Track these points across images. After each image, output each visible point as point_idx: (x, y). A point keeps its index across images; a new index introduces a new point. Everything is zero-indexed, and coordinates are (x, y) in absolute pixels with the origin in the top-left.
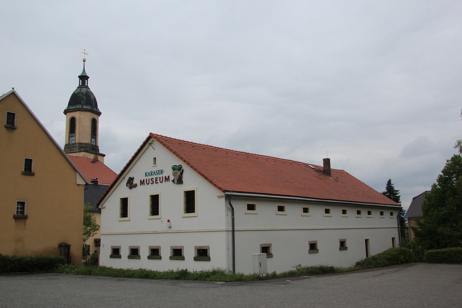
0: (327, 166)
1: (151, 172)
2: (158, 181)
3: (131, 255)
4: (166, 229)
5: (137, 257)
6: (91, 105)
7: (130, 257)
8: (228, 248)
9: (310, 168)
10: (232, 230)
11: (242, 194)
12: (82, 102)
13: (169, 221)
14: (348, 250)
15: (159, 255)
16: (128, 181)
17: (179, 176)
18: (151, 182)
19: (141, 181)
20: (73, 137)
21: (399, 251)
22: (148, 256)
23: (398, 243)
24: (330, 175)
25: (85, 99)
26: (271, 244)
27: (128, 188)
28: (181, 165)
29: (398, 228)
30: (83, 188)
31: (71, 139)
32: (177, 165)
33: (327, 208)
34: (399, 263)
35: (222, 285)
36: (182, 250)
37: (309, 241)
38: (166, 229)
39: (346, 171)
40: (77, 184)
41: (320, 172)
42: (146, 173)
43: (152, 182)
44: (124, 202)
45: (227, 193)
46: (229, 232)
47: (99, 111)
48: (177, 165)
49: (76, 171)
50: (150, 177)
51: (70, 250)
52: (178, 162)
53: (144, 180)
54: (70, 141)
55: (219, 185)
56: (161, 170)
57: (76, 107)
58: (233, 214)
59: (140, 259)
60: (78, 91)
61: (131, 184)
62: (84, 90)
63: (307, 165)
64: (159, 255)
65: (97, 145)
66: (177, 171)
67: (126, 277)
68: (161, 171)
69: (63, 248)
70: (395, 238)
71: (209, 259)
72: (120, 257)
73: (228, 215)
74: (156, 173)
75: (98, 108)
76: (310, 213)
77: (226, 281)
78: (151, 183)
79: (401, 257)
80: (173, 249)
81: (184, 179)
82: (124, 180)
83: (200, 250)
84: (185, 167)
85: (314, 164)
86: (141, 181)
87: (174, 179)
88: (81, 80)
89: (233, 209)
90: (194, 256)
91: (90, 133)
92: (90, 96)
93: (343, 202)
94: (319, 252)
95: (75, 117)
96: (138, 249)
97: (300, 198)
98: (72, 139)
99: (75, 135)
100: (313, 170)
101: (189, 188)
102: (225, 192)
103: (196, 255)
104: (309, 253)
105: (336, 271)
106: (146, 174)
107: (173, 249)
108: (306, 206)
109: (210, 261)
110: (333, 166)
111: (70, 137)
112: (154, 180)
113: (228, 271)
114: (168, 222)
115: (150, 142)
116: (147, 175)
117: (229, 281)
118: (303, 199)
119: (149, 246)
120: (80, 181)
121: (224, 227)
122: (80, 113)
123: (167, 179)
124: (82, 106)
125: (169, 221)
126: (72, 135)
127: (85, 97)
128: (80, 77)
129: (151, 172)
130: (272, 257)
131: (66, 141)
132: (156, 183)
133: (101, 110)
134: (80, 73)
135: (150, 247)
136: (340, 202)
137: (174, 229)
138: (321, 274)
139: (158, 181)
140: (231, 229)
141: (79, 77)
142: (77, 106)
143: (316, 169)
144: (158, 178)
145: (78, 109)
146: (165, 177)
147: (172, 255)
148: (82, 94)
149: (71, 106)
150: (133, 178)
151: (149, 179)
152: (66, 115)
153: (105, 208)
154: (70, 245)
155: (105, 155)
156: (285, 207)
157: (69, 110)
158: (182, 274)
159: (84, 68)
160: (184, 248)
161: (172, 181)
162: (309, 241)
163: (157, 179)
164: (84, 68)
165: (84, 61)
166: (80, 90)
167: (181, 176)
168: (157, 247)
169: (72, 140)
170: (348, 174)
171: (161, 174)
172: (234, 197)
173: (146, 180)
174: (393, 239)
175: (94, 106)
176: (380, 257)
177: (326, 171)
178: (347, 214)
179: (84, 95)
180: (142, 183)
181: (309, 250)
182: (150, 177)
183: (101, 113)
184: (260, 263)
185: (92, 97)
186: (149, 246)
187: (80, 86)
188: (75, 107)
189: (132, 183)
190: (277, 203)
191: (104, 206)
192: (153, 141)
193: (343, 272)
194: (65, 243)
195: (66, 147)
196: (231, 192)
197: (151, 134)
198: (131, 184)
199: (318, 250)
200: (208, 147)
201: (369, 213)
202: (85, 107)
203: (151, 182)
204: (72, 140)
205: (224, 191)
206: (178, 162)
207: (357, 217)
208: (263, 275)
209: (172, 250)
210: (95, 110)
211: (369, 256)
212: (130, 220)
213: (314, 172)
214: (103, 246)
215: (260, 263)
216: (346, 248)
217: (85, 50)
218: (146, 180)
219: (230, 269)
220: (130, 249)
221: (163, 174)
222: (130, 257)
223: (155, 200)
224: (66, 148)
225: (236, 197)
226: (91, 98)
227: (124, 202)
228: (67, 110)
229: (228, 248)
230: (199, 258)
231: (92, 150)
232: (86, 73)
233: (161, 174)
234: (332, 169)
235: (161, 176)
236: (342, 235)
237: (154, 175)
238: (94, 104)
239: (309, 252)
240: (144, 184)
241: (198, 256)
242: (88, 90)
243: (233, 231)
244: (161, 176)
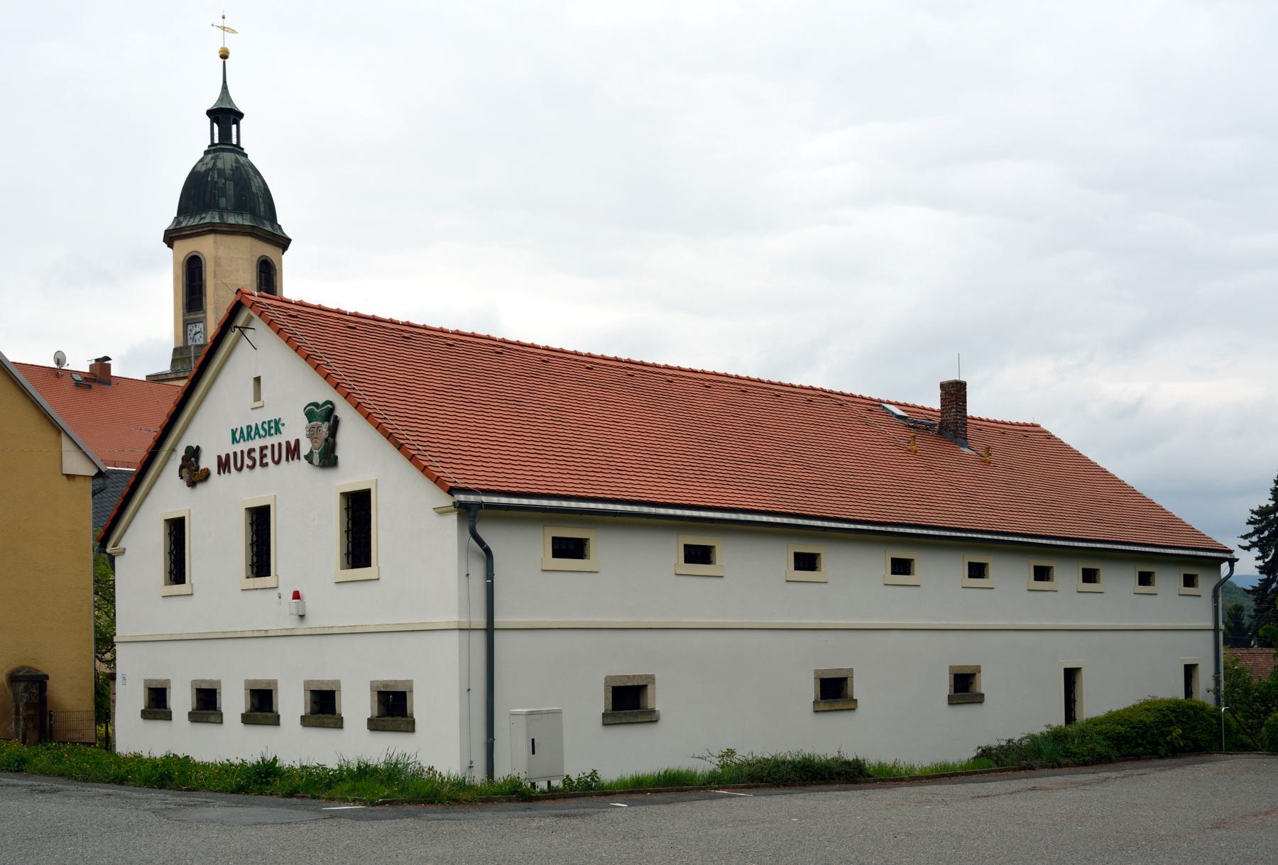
0: (952, 408)
1: (248, 427)
2: (268, 460)
3: (197, 709)
4: (290, 623)
5: (212, 718)
6: (253, 213)
7: (247, 719)
8: (469, 690)
9: (890, 414)
10: (485, 627)
11: (534, 502)
12: (223, 201)
13: (296, 595)
14: (985, 702)
15: (271, 711)
16: (183, 459)
17: (326, 440)
18: (248, 462)
19: (219, 457)
20: (198, 324)
21: (1168, 712)
22: (244, 712)
23: (1212, 685)
24: (964, 441)
25: (232, 192)
26: (651, 678)
27: (182, 484)
28: (331, 403)
29: (1216, 630)
30: (88, 487)
31: (191, 331)
32: (321, 403)
33: (1146, 568)
34: (1162, 753)
35: (355, 817)
36: (336, 692)
37: (816, 671)
38: (290, 623)
39: (1044, 426)
40: (64, 472)
41: (927, 429)
42: (232, 430)
43: (250, 463)
44: (176, 529)
45: (462, 498)
46: (472, 632)
47: (283, 233)
48: (321, 403)
49: (59, 430)
50: (244, 446)
51: (48, 693)
52: (322, 393)
53: (228, 456)
54: (189, 336)
55: (438, 470)
56: (275, 420)
57: (201, 219)
58: (490, 573)
59: (221, 722)
60: (207, 164)
61: (193, 473)
62: (227, 159)
63: (880, 406)
64: (274, 709)
66: (320, 423)
67: (109, 783)
68: (277, 422)
69: (21, 686)
70: (1200, 667)
71: (409, 727)
72: (338, 724)
73: (468, 575)
74: (262, 433)
75: (279, 223)
76: (1055, 581)
77: (373, 804)
78: (248, 466)
79: (1170, 733)
80: (313, 692)
81: (340, 452)
82: (173, 457)
83: (388, 693)
84: (344, 411)
85: (910, 402)
86: (219, 457)
87: (311, 452)
88: (216, 126)
89: (488, 552)
90: (369, 716)
92: (249, 179)
93: (970, 535)
94: (857, 710)
95: (202, 255)
96: (216, 690)
97: (778, 520)
98: (194, 332)
99: (205, 318)
100: (901, 421)
101: (354, 483)
102: (455, 496)
103: (376, 713)
104: (816, 711)
105: (869, 776)
106: (234, 433)
107: (312, 692)
108: (978, 558)
109: (413, 731)
110: (975, 407)
111: (186, 324)
112: (257, 455)
113: (356, 765)
114: (294, 598)
115: (240, 321)
116: (238, 439)
117: (383, 804)
118: (793, 521)
119: (246, 681)
120: (75, 463)
121: (452, 617)
122: (215, 242)
123: (293, 451)
124: (221, 217)
125: (296, 595)
126: (193, 316)
127: (230, 185)
128: (215, 115)
129: (248, 427)
130: (656, 721)
131: (176, 337)
132: (264, 465)
133: (288, 231)
134: (211, 101)
135: (247, 682)
136: (990, 537)
137: (316, 621)
138: (748, 787)
139: (268, 460)
140: (480, 621)
141: (210, 113)
142: (204, 215)
143: (914, 421)
144: (266, 447)
145: (210, 228)
146: (288, 443)
147: (309, 710)
148: (221, 173)
149: (185, 218)
150: (198, 448)
151: (242, 452)
152: (172, 247)
153: (123, 552)
154: (46, 677)
156: (822, 555)
157: (181, 231)
158: (259, 774)
159: (225, 82)
160: (414, 690)
161: (307, 457)
162: (816, 671)
163: (264, 452)
164: (225, 82)
165: (224, 56)
166: (212, 159)
167: (330, 438)
168: (269, 682)
169: (195, 334)
170: (1049, 437)
171: (276, 433)
172: (488, 511)
173: (235, 454)
174: (1190, 670)
175: (262, 214)
176: (1083, 731)
177: (948, 426)
178: (1052, 581)
179: (226, 179)
180: (223, 465)
181: (814, 702)
182: (244, 446)
183: (290, 240)
184: (533, 740)
185: (255, 183)
186: (246, 681)
187: (213, 148)
188: (197, 220)
189: (193, 465)
190: (680, 536)
191: (121, 545)
192: (250, 319)
193: (902, 780)
194: (29, 669)
195: (178, 357)
196: (478, 494)
197: (239, 293)
198: (193, 473)
199: (856, 700)
200: (426, 332)
201: (1090, 576)
202: (232, 220)
203: (248, 462)
204: (195, 334)
205: (451, 491)
206: (322, 393)
207: (1030, 589)
208: (549, 782)
209: (309, 692)
210: (269, 228)
212: (192, 594)
213: (901, 434)
214: (124, 679)
215: (533, 740)
216: (979, 699)
217: (224, 17)
218: (235, 454)
219: (472, 759)
220: (195, 690)
221: (280, 433)
222: (247, 719)
223: (260, 519)
224: (176, 359)
225: (503, 512)
226: (254, 187)
227: (176, 529)
228: (173, 233)
229: (469, 690)
230: (383, 721)
232: (230, 101)
233: (276, 433)
234: (973, 419)
235: (274, 440)
236: (964, 654)
237: (257, 436)
238: (262, 209)
239: (817, 709)
240: (229, 472)
241: (384, 716)
242: (241, 159)
243: (490, 630)
244: (274, 440)
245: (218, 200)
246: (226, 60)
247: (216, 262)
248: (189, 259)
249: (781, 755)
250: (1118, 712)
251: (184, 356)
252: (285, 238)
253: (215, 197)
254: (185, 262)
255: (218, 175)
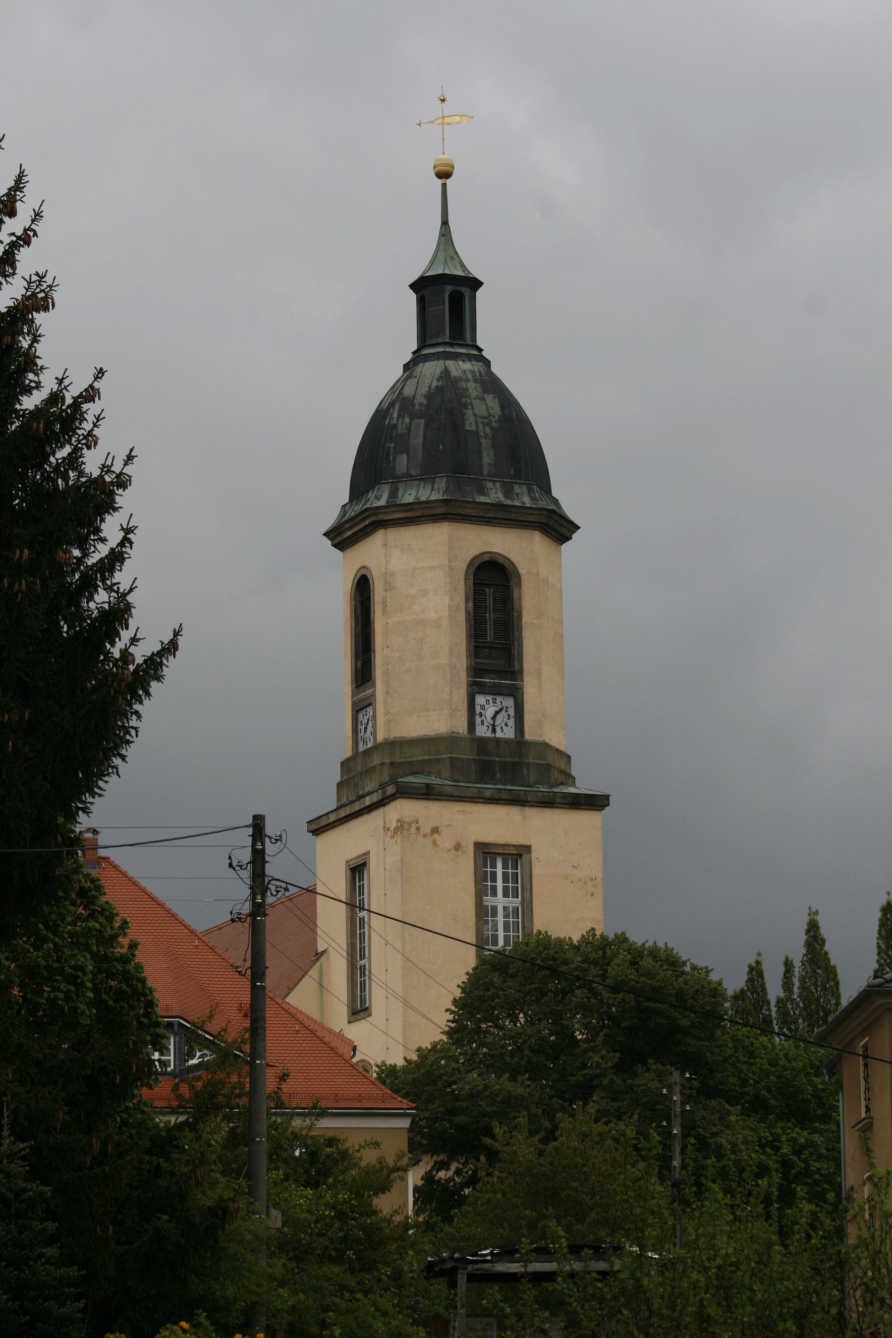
12: (402, 463)
25: (420, 440)
65: (530, 735)
91: (462, 662)
155: (607, 797)
159: (445, 223)
164: (445, 223)
165: (444, 175)
211: (474, 943)
231: (481, 780)
238: (487, 460)
245: (394, 458)
246: (448, 181)
247: (386, 582)
248: (358, 581)
249: (212, 1116)
250: (560, 942)
251: (353, 774)
252: (562, 516)
253: (388, 455)
254: (354, 587)
255: (400, 411)
